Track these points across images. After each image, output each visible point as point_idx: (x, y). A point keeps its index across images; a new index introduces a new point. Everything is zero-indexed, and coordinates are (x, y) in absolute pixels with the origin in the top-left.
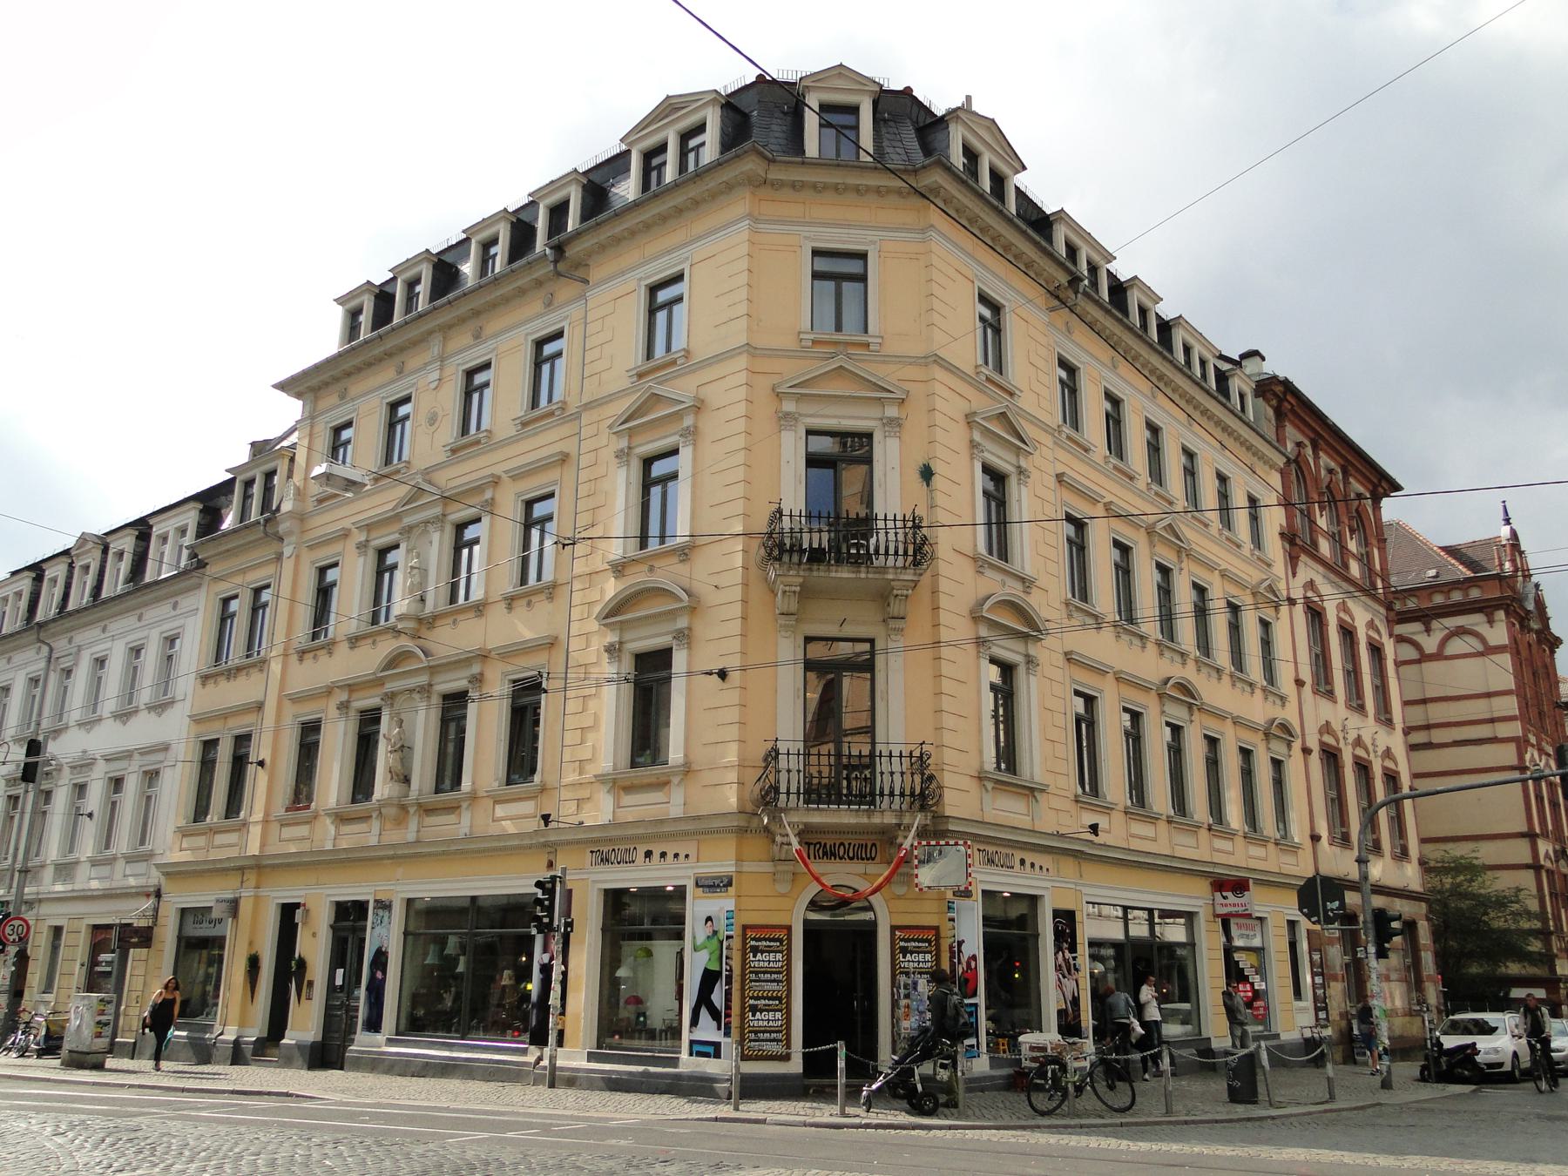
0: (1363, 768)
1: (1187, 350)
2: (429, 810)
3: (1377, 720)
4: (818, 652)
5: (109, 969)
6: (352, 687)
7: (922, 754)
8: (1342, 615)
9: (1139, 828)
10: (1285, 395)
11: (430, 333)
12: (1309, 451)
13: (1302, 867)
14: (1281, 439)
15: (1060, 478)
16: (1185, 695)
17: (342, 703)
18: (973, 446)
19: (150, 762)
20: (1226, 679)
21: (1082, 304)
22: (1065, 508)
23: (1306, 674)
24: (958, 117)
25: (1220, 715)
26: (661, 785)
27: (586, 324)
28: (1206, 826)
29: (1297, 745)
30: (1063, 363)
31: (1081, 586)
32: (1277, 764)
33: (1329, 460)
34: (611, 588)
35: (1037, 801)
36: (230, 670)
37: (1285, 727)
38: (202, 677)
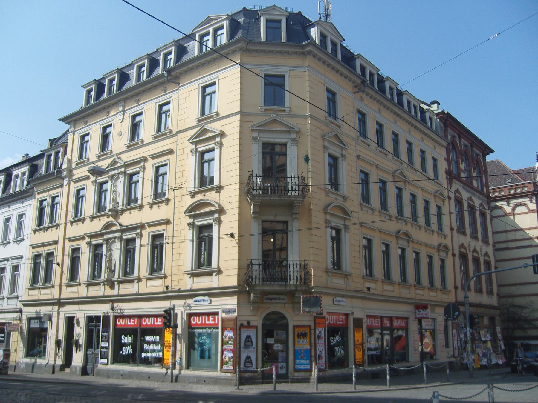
0: (476, 260)
1: (409, 102)
2: (120, 282)
3: (483, 241)
4: (267, 225)
5: (3, 339)
6: (92, 236)
7: (304, 264)
8: (470, 202)
9: (387, 287)
10: (447, 118)
11: (120, 100)
12: (457, 139)
13: (451, 298)
14: (446, 136)
15: (358, 157)
16: (406, 237)
17: (88, 242)
18: (325, 148)
19: (15, 263)
20: (423, 230)
21: (367, 90)
22: (360, 168)
23: (454, 225)
24: (318, 24)
25: (420, 244)
26: (210, 274)
27: (179, 100)
28: (413, 285)
29: (450, 253)
30: (360, 112)
31: (366, 198)
32: (443, 261)
33: (465, 142)
34: (189, 201)
35: (348, 279)
36: (44, 228)
37: (446, 247)
38: (34, 230)
